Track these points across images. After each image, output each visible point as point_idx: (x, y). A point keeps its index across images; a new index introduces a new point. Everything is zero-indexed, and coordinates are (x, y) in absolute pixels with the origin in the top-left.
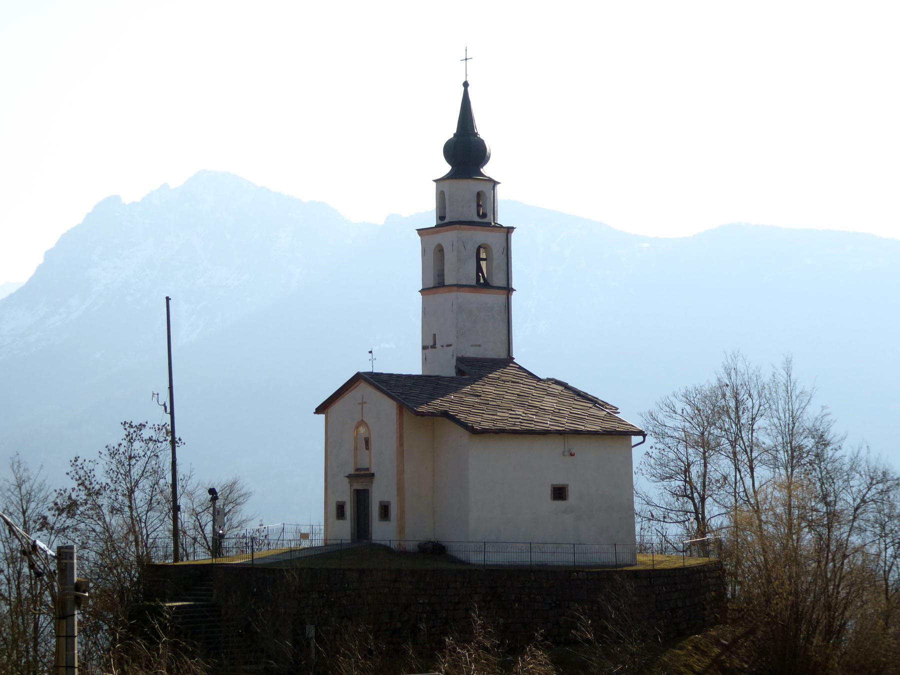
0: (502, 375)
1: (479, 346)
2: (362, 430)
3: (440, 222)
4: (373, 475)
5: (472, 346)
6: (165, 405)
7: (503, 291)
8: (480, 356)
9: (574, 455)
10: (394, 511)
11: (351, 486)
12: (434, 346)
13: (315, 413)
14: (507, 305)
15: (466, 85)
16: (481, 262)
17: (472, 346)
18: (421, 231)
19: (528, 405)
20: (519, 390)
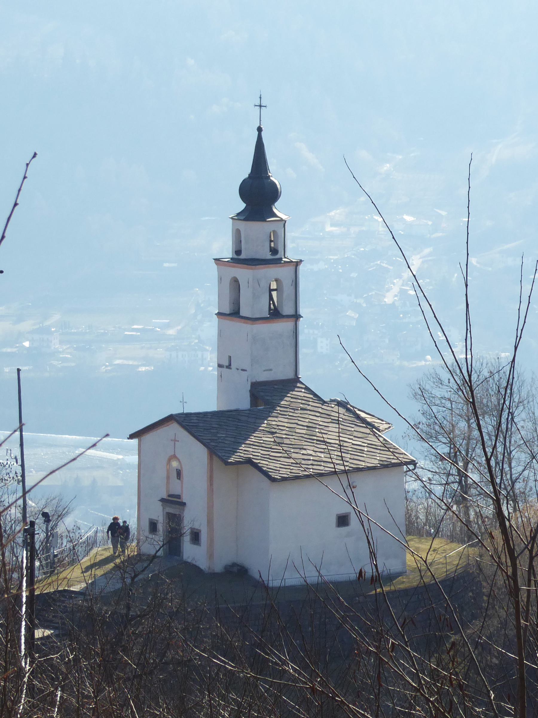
0: (292, 400)
1: (271, 370)
2: (175, 464)
3: (236, 257)
4: (184, 504)
5: (264, 371)
6: (16, 458)
7: (292, 319)
8: (271, 379)
9: (355, 487)
10: (204, 537)
11: (163, 508)
12: (229, 367)
14: (295, 331)
15: (260, 130)
16: (272, 292)
17: (264, 371)
19: (317, 440)
20: (307, 420)
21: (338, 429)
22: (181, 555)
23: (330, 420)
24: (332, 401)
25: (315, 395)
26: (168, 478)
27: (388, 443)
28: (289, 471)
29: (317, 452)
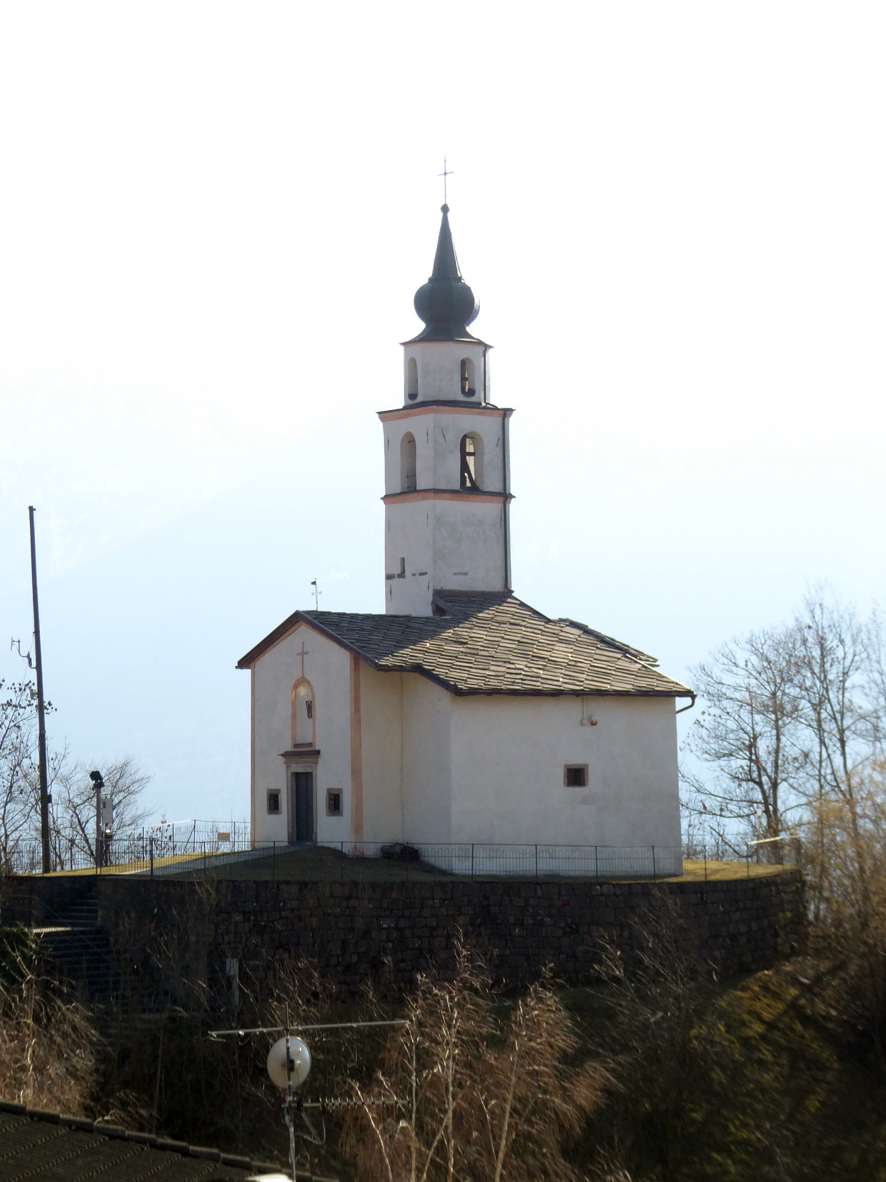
0: (496, 614)
1: (466, 574)
2: (303, 691)
4: (318, 753)
5: (455, 574)
6: (28, 656)
9: (596, 724)
10: (347, 802)
12: (402, 575)
13: (237, 667)
15: (445, 209)
16: (467, 457)
17: (455, 574)
18: (382, 415)
19: (533, 656)
20: (520, 635)
21: (594, 861)
22: (314, 837)
23: (557, 639)
24: (561, 620)
25: (536, 612)
26: (294, 716)
27: (649, 670)
28: (483, 682)
29: (531, 667)
